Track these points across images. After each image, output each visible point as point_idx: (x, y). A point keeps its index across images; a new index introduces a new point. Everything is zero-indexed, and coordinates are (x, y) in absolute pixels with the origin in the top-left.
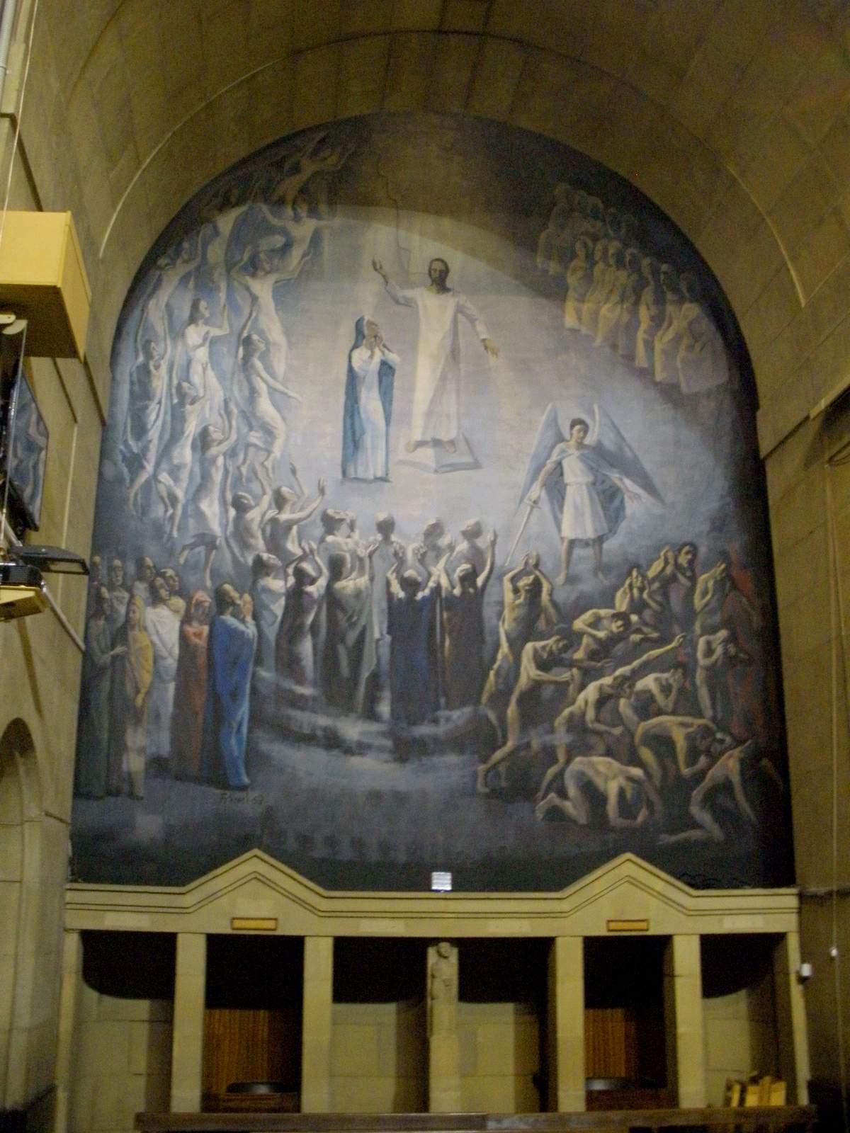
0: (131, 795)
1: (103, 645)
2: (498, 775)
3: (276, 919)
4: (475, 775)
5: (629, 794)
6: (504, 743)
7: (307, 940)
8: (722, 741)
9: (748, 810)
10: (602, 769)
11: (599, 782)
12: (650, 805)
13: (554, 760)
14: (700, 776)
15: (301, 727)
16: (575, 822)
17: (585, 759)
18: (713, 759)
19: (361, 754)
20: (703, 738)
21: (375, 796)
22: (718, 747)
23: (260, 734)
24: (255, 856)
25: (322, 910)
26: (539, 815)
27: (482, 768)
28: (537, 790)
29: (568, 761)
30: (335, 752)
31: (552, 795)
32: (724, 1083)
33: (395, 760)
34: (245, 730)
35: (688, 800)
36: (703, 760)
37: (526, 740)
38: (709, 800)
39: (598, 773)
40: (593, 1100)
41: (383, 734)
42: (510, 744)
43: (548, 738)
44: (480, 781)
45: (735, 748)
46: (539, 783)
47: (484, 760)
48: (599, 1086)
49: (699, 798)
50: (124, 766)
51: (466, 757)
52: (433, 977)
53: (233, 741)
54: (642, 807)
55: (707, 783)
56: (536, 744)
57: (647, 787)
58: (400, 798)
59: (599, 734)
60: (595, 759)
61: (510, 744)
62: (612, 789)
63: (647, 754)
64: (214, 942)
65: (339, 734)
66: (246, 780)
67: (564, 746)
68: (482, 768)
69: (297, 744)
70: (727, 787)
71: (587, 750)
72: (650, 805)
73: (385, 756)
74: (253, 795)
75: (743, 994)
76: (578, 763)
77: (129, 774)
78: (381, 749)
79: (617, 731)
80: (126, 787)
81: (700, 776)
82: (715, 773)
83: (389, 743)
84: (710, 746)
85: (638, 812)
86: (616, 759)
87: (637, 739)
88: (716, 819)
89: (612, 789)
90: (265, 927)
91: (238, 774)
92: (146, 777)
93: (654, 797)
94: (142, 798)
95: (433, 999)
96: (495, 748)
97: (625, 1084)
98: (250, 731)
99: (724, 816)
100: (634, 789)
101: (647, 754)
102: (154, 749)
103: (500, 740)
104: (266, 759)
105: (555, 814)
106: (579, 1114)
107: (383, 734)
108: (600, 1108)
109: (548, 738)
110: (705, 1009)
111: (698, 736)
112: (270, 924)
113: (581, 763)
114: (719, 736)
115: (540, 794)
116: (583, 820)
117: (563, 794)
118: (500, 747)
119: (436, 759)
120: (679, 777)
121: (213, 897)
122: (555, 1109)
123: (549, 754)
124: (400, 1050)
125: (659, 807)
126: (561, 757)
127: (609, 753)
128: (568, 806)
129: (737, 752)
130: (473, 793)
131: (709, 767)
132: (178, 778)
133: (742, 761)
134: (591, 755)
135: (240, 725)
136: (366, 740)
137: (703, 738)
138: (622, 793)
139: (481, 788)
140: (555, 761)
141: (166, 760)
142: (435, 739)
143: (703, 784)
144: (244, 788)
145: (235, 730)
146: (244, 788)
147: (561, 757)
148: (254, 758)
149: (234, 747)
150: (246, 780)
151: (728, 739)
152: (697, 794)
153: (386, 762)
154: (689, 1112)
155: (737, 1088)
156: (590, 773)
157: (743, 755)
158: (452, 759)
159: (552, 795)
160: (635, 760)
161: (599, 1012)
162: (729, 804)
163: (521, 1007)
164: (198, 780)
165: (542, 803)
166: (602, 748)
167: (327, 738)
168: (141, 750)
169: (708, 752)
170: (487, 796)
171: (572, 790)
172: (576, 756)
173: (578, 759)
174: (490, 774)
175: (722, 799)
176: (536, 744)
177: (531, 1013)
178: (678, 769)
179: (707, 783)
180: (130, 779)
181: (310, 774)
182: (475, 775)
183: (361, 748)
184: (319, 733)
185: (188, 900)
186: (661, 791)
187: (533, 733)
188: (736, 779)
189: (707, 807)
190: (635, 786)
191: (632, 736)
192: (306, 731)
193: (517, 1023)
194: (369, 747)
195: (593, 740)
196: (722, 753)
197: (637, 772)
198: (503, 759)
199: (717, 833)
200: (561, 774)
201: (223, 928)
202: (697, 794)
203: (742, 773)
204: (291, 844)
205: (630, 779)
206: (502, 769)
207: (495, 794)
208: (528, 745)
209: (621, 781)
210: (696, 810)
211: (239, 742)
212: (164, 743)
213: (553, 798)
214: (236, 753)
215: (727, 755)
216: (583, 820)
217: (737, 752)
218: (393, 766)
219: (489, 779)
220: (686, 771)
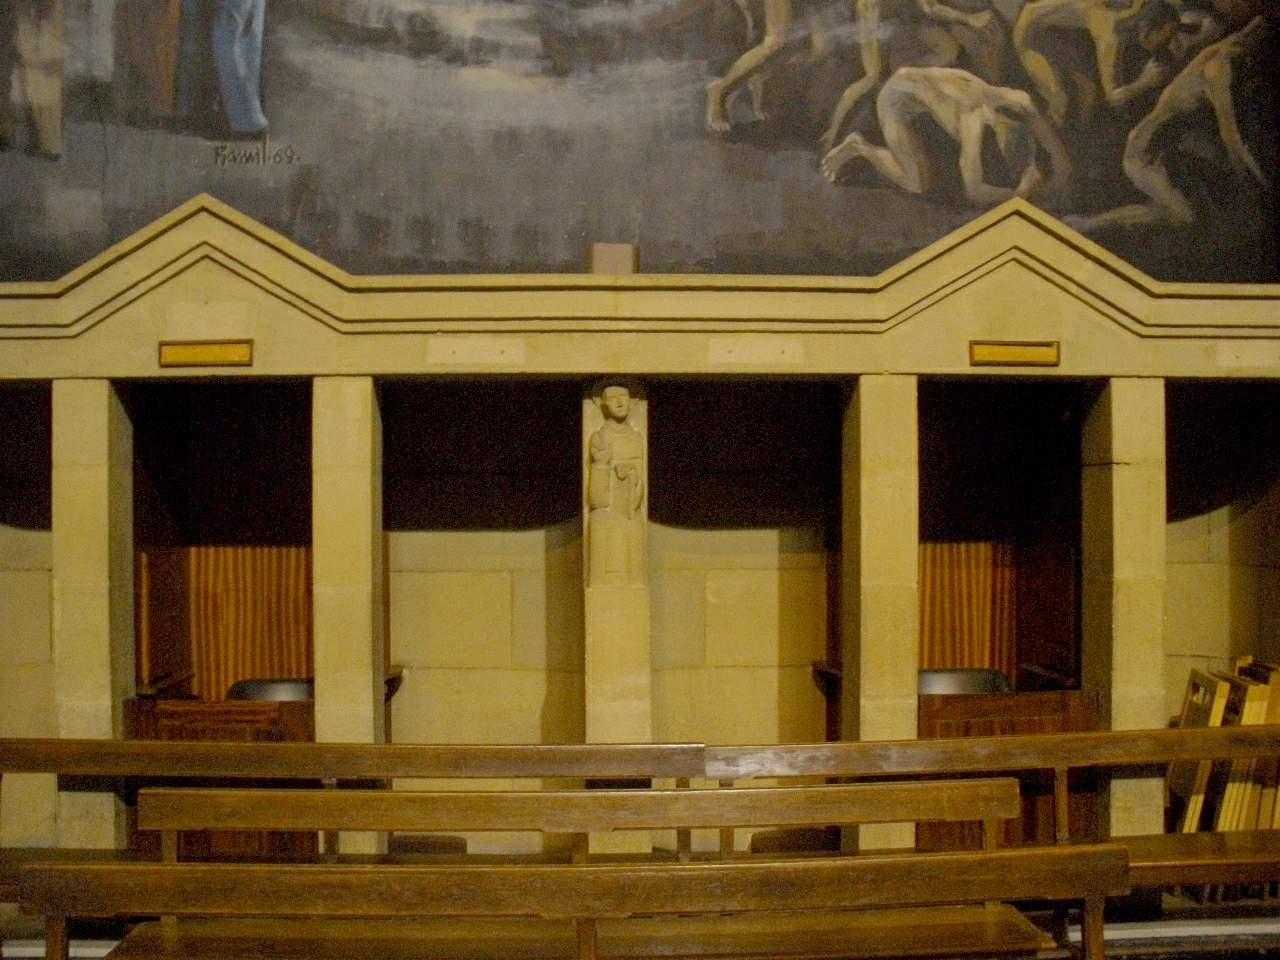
0: (34, 148)
1: (1053, 945)
2: (746, 98)
3: (249, 342)
4: (702, 98)
5: (1002, 140)
6: (759, 40)
7: (318, 385)
8: (1193, 29)
9: (1249, 160)
10: (948, 89)
11: (944, 115)
12: (1044, 160)
13: (860, 74)
14: (1144, 102)
15: (365, 17)
16: (897, 189)
17: (913, 70)
18: (1173, 66)
19: (479, 63)
20: (1155, 25)
21: (508, 140)
22: (1185, 41)
23: (286, 33)
24: (203, 209)
25: (346, 317)
26: (829, 174)
27: (715, 85)
28: (824, 126)
29: (886, 73)
30: (432, 59)
31: (854, 137)
32: (1186, 677)
33: (545, 72)
34: (258, 26)
35: (1120, 146)
36: (1151, 70)
37: (802, 33)
38: (1163, 146)
39: (941, 96)
40: (932, 716)
41: (521, 24)
42: (771, 41)
43: (843, 31)
44: (712, 108)
45: (1225, 35)
46: (826, 116)
47: (721, 72)
48: (942, 686)
49: (1143, 142)
50: (15, 94)
51: (684, 64)
52: (592, 460)
53: (237, 50)
54: (1028, 165)
55: (1158, 115)
56: (820, 42)
57: (1041, 127)
58: (557, 143)
59: (945, 24)
60: (936, 71)
61: (771, 41)
62: (970, 130)
63: (1036, 64)
64: (132, 394)
65: (437, 27)
66: (262, 120)
67: (875, 45)
68: (715, 85)
69: (356, 51)
70: (1204, 114)
71: (920, 55)
72: (1044, 160)
73: (527, 65)
74: (273, 147)
75: (1221, 516)
76: (904, 79)
77: (28, 110)
78: (518, 52)
79: (980, 20)
80: (20, 136)
81: (1144, 102)
82: (1180, 92)
83: (533, 41)
84: (1168, 41)
85: (1020, 175)
86: (976, 74)
87: (1018, 36)
88: (1175, 178)
89: (970, 130)
90: (209, 359)
91: (248, 110)
92: (67, 112)
93: (1052, 146)
94: (56, 157)
95: (592, 509)
96: (743, 47)
97: (992, 682)
98: (267, 30)
99: (1184, 173)
100: (1013, 130)
101: (1036, 64)
102: (80, 66)
103: (751, 34)
104: (300, 80)
105: (858, 173)
106: (904, 744)
107: (521, 24)
108: (947, 732)
109: (843, 31)
110: (1168, 535)
111: (1142, 23)
112: (238, 353)
113: (909, 78)
114: (1186, 18)
115: (830, 135)
116: (913, 186)
117: (875, 137)
118: (752, 46)
119: (625, 70)
120: (1102, 107)
121: (119, 301)
122: (855, 736)
123: (848, 61)
124: (919, 572)
125: (1061, 163)
126: (871, 64)
127: (963, 60)
128: (884, 159)
129: (1225, 47)
130: (703, 133)
131: (1165, 82)
132: (131, 120)
133: (1237, 64)
134: (928, 65)
135: (249, 24)
136: (489, 36)
137: (1155, 25)
138: (988, 134)
139: (714, 123)
140: (860, 74)
141: (108, 87)
142: (626, 33)
143: (1151, 116)
144: (258, 136)
145: (241, 28)
146: (258, 136)
147: (871, 64)
148: (276, 78)
149: (239, 58)
150: (262, 120)
151: (1207, 22)
152: (1138, 137)
153: (528, 75)
154: (1129, 738)
155: (1224, 689)
156: (927, 97)
157: (1238, 50)
158: (655, 68)
159: (854, 137)
160: (1012, 74)
161: (944, 548)
162: (1207, 152)
163: (791, 534)
164: (172, 125)
165: (834, 152)
166: (950, 51)
167: (413, 32)
168: (52, 67)
169: (1162, 54)
170: (727, 138)
171: (892, 128)
172: (898, 66)
173: (903, 71)
174: (731, 98)
175: (1188, 143)
176: (820, 42)
177: (814, 549)
178: (1100, 89)
179: (1158, 115)
180: (30, 118)
181: (381, 102)
182: (702, 98)
183: (480, 52)
184: (400, 27)
185: (67, 309)
186: (1068, 131)
187: (815, 21)
188: (1222, 101)
189: (1157, 163)
190: (1016, 124)
191: (1008, 30)
192: (375, 23)
193: (782, 568)
194: (496, 48)
195: (931, 35)
196: (1191, 53)
197: (1019, 98)
198: (757, 69)
199: (1179, 208)
200: (869, 99)
201: (146, 367)
202: (1138, 137)
203: (1235, 87)
204: (347, 233)
205: (1005, 111)
206: (755, 85)
207: (740, 133)
208: (806, 43)
209: (987, 113)
210: (1133, 167)
211: (248, 51)
212: (102, 57)
213: (855, 141)
214: (242, 70)
215: (1204, 53)
216: (913, 186)
217: (1225, 47)
218: (543, 81)
219: (728, 106)
220: (1116, 94)
